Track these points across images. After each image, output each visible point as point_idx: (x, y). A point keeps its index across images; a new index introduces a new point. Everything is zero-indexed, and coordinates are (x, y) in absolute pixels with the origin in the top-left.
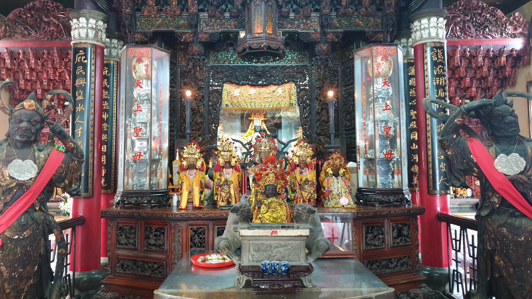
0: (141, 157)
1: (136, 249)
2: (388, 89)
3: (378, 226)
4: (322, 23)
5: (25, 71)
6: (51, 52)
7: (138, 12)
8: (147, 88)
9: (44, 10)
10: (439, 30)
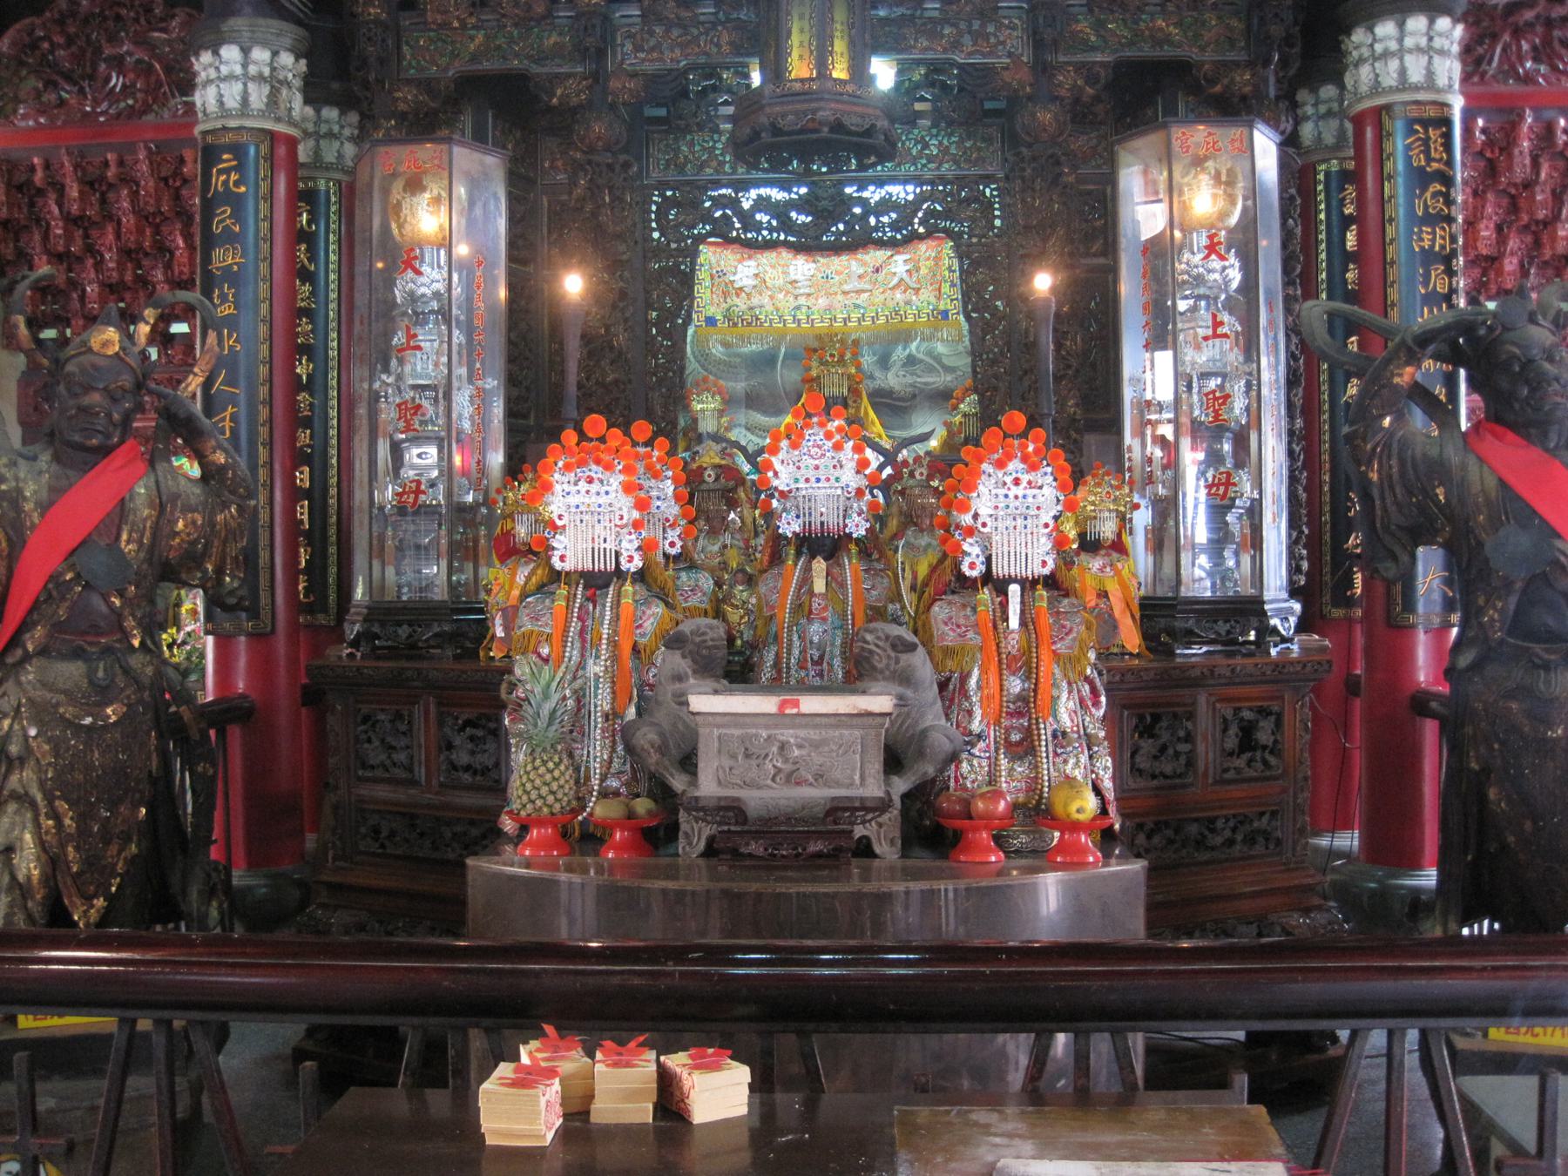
0: (423, 497)
1: (413, 783)
2: (1224, 268)
3: (1175, 715)
4: (1035, 33)
5: (48, 224)
6: (128, 158)
7: (407, 14)
8: (435, 275)
9: (105, 19)
10: (1437, 60)
